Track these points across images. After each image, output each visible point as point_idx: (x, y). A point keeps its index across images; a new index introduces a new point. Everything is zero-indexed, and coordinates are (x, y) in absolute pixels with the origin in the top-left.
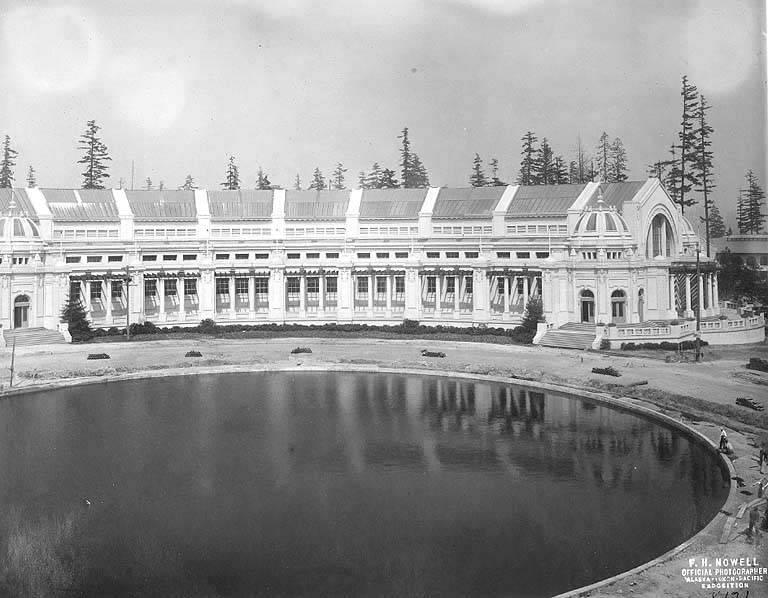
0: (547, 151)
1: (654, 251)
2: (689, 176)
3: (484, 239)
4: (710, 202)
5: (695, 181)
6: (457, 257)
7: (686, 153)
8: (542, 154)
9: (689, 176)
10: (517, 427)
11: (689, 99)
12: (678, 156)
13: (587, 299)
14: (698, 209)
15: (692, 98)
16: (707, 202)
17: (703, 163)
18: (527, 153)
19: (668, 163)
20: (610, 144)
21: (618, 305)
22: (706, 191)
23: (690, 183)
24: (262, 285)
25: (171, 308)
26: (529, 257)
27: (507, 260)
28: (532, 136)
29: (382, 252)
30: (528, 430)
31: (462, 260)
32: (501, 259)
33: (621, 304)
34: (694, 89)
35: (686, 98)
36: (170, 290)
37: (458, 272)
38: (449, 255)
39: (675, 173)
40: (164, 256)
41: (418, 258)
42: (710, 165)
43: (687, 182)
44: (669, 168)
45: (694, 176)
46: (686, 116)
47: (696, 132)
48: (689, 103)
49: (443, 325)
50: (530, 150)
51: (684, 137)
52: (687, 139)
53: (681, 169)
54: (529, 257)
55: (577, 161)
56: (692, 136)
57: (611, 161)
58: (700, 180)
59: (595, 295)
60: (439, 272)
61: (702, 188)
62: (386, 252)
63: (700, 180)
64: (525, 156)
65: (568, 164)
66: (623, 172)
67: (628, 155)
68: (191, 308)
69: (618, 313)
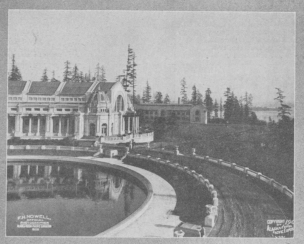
0: (159, 95)
1: (36, 109)
2: (128, 81)
3: (52, 103)
4: (135, 91)
5: (131, 83)
7: (128, 73)
8: (74, 70)
9: (128, 81)
11: (130, 53)
12: (126, 74)
13: (105, 127)
15: (131, 53)
17: (133, 76)
18: (66, 69)
19: (122, 76)
20: (100, 67)
21: (104, 129)
22: (133, 87)
23: (129, 84)
24: (44, 119)
25: (34, 131)
26: (40, 110)
28: (68, 62)
29: (37, 108)
33: (106, 129)
34: (131, 50)
35: (129, 53)
39: (125, 80)
40: (26, 109)
41: (23, 112)
42: (135, 77)
43: (128, 83)
44: (123, 78)
46: (129, 59)
47: (132, 65)
48: (130, 54)
50: (67, 67)
51: (128, 67)
52: (129, 67)
54: (40, 110)
55: (88, 73)
56: (130, 67)
57: (100, 74)
58: (132, 82)
60: (31, 115)
61: (132, 86)
62: (39, 108)
64: (65, 70)
65: (85, 74)
66: (105, 78)
67: (106, 72)
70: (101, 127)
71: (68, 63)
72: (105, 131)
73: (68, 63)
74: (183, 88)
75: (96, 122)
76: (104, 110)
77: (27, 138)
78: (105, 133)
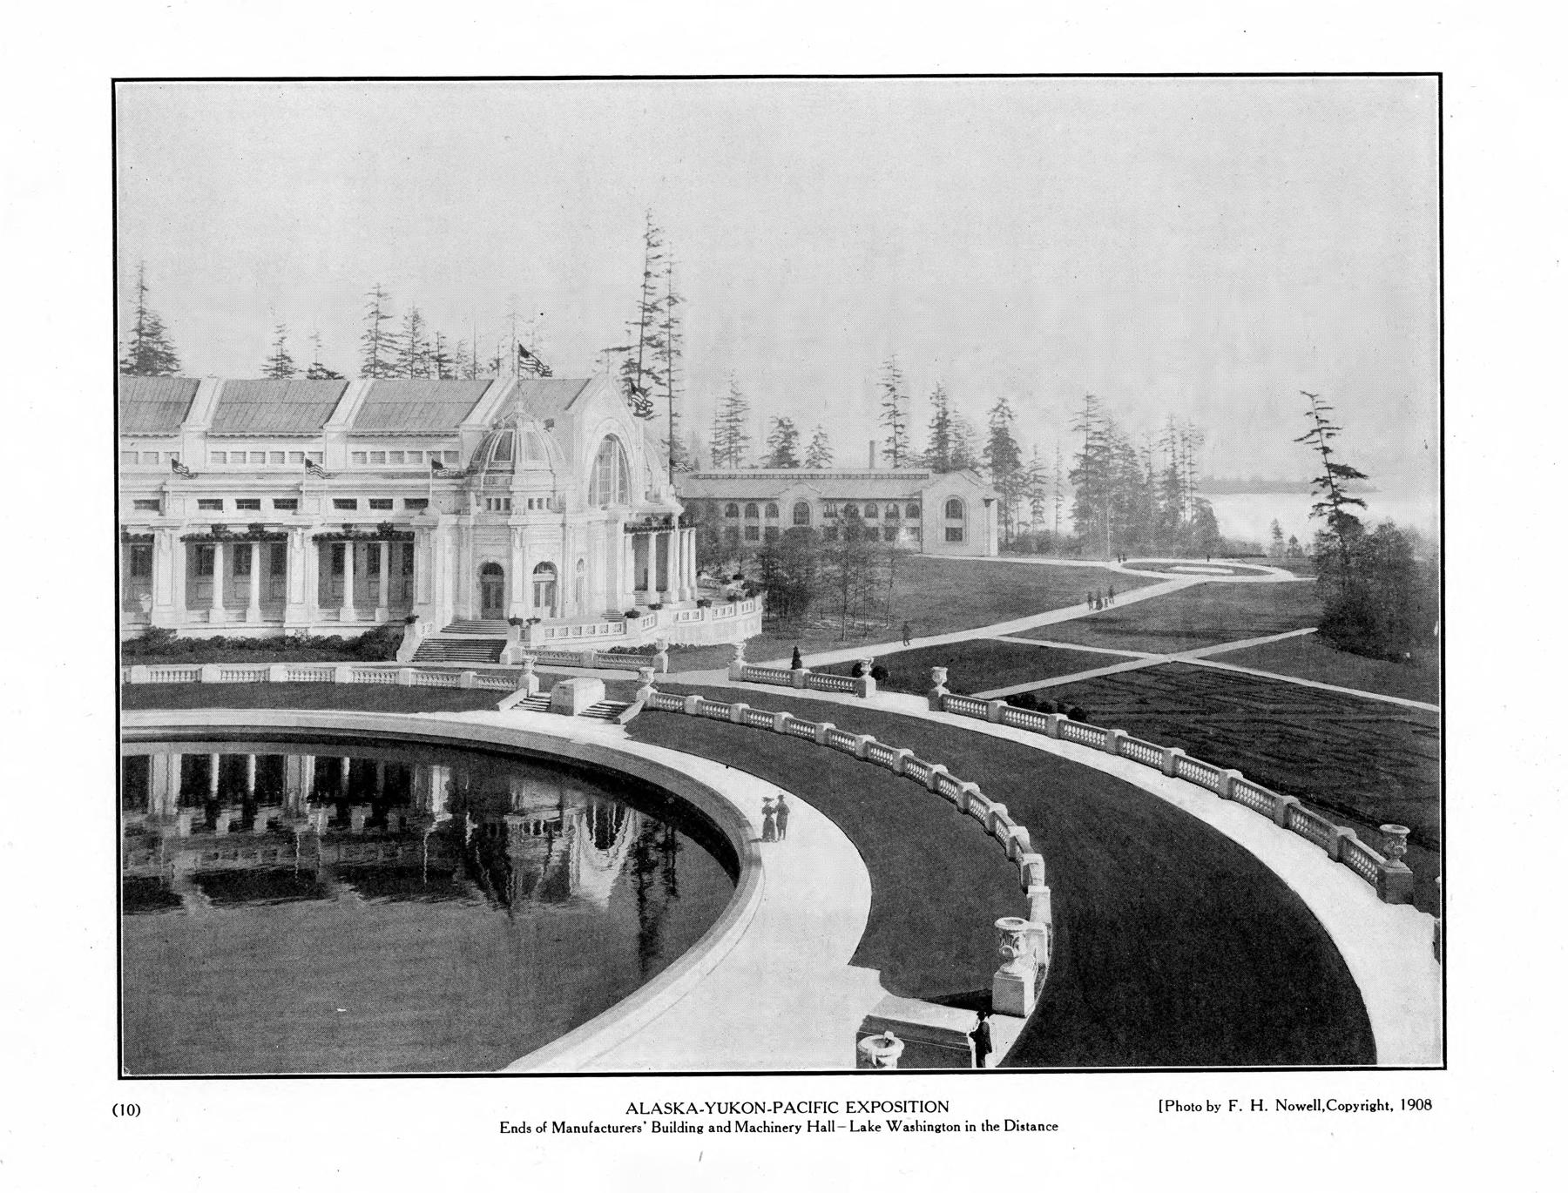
6: (478, 505)
10: (360, 816)
14: (660, 426)
16: (671, 415)
25: (238, 603)
27: (254, 512)
30: (377, 820)
31: (269, 516)
32: (376, 512)
36: (241, 567)
37: (257, 531)
38: (375, 504)
45: (655, 371)
49: (226, 634)
53: (637, 361)
54: (221, 508)
56: (654, 308)
59: (559, 568)
62: (215, 497)
63: (665, 378)
68: (275, 600)
69: (493, 602)
70: (530, 578)
71: (379, 295)
72: (547, 594)
73: (379, 295)
74: (890, 400)
75: (509, 556)
76: (540, 501)
77: (206, 635)
78: (547, 603)
